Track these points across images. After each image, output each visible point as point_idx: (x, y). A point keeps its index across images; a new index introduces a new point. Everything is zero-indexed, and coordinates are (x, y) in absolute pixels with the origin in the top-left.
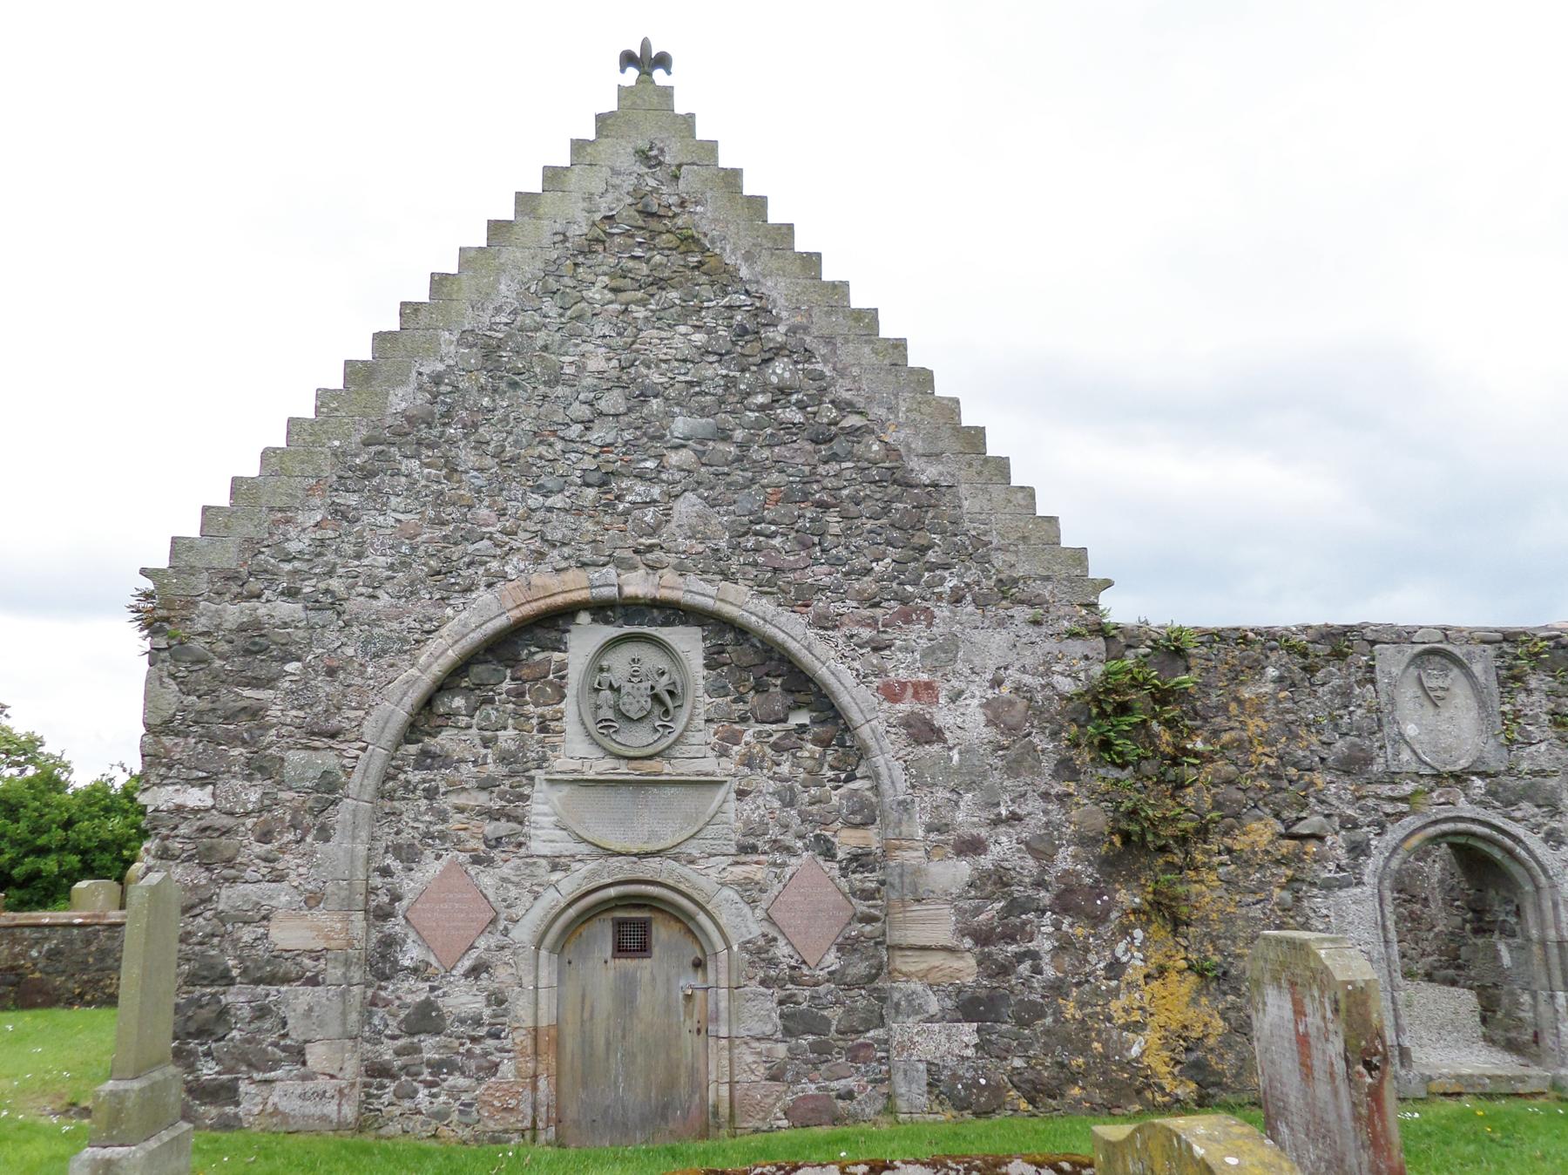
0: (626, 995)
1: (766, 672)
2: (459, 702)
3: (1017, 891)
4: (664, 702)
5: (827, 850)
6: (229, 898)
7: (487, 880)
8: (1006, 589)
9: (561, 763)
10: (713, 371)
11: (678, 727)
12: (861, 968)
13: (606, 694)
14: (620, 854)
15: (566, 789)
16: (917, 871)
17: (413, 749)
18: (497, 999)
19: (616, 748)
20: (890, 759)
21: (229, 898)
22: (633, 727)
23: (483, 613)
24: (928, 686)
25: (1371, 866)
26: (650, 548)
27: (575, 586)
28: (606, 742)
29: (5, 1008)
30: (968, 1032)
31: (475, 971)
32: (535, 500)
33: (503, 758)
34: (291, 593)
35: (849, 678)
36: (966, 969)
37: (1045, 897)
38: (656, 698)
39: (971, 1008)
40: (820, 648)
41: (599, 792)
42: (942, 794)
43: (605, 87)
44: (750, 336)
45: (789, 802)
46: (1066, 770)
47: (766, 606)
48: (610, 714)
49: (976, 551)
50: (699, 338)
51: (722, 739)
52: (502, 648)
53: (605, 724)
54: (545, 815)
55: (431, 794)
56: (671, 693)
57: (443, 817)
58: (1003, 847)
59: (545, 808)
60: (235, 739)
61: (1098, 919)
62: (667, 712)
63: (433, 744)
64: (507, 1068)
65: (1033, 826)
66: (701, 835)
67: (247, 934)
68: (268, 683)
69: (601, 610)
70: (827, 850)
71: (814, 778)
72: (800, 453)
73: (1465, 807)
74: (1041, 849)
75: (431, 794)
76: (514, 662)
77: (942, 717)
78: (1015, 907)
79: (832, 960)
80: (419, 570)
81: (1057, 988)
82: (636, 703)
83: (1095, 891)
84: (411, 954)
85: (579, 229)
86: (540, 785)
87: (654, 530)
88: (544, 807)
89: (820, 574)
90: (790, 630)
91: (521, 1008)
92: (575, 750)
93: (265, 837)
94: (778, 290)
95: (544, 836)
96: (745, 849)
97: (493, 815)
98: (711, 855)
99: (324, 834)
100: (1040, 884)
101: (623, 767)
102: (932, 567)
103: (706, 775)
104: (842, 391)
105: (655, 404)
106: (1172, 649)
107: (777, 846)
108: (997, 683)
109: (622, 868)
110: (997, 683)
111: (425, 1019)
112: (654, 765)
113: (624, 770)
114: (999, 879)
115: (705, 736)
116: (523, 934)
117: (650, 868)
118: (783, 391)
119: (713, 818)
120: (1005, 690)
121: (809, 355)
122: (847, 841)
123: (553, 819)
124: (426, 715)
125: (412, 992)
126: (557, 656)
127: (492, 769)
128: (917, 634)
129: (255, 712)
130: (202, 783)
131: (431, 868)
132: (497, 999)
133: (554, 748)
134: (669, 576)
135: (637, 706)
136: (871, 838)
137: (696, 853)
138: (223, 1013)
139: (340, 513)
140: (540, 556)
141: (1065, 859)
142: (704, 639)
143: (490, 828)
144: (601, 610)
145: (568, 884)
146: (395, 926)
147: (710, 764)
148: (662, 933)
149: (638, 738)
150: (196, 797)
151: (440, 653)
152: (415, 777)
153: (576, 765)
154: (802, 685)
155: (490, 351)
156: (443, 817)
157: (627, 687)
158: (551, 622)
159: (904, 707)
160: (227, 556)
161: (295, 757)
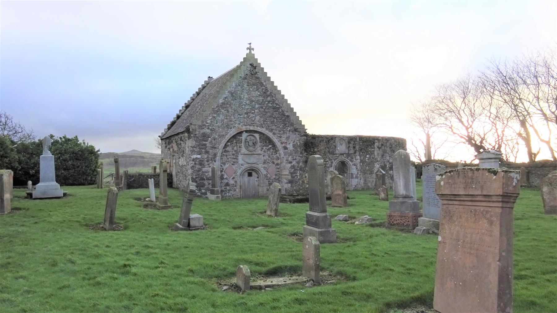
0: (249, 182)
1: (267, 141)
4: (254, 144)
5: (273, 163)
6: (204, 169)
7: (234, 167)
8: (296, 130)
9: (242, 152)
10: (261, 98)
12: (277, 177)
18: (236, 182)
20: (281, 151)
21: (204, 169)
23: (233, 132)
27: (244, 128)
29: (509, 188)
30: (290, 185)
31: (233, 178)
32: (239, 116)
33: (235, 151)
34: (208, 128)
36: (290, 177)
39: (290, 182)
43: (244, 53)
45: (269, 157)
46: (301, 153)
47: (267, 132)
49: (292, 125)
52: (234, 137)
55: (226, 156)
57: (228, 159)
58: (294, 163)
60: (203, 149)
61: (304, 171)
64: (237, 190)
65: (297, 160)
67: (206, 174)
68: (207, 141)
69: (246, 131)
70: (273, 163)
71: (272, 154)
73: (343, 158)
74: (298, 163)
75: (226, 156)
76: (236, 138)
77: (288, 146)
78: (296, 170)
79: (274, 177)
81: (299, 179)
82: (251, 143)
83: (304, 168)
84: (225, 176)
85: (243, 76)
87: (254, 121)
88: (240, 157)
89: (274, 127)
90: (270, 135)
91: (238, 182)
92: (244, 150)
93: (208, 161)
94: (269, 86)
95: (240, 161)
96: (264, 163)
97: (234, 159)
99: (215, 161)
104: (277, 102)
106: (314, 137)
107: (268, 163)
109: (250, 165)
111: (227, 184)
113: (250, 153)
114: (293, 167)
115: (259, 148)
116: (238, 174)
117: (253, 165)
118: (269, 102)
119: (259, 158)
121: (273, 96)
122: (276, 162)
125: (226, 181)
127: (234, 152)
128: (285, 136)
129: (205, 145)
131: (227, 166)
132: (236, 182)
134: (256, 127)
136: (279, 161)
138: (204, 184)
139: (214, 117)
140: (239, 124)
141: (301, 164)
143: (234, 160)
144: (246, 131)
145: (243, 168)
146: (223, 173)
147: (260, 152)
148: (254, 173)
149: (251, 148)
150: (199, 156)
151: (228, 137)
154: (271, 142)
155: (232, 94)
156: (228, 159)
158: (240, 133)
161: (211, 151)
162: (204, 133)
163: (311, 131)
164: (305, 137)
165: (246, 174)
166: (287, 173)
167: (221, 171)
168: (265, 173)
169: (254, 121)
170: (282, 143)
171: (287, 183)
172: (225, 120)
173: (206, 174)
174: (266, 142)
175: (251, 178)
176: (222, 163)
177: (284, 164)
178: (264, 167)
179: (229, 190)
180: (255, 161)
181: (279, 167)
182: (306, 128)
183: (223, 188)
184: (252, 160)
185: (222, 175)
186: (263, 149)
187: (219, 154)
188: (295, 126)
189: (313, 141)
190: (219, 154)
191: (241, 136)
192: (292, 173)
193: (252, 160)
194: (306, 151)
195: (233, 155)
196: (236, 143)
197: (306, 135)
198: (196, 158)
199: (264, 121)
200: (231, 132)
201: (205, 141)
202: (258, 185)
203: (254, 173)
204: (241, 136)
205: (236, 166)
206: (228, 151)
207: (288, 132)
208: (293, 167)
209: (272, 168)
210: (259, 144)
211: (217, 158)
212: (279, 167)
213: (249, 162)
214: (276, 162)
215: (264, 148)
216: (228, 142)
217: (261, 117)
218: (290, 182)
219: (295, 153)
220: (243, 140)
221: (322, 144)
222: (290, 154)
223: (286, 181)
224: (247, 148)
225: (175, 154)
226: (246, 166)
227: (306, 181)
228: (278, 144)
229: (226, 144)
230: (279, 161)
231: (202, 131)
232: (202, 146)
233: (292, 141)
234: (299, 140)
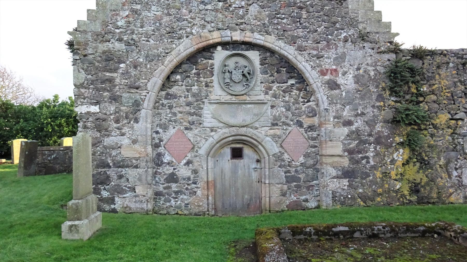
0: (234, 171)
3: (363, 138)
4: (247, 76)
5: (300, 124)
6: (108, 141)
7: (190, 135)
8: (363, 37)
9: (213, 97)
11: (252, 85)
12: (311, 162)
13: (227, 74)
14: (233, 126)
15: (215, 106)
17: (164, 93)
18: (195, 172)
19: (231, 92)
20: (322, 94)
21: (108, 141)
22: (236, 84)
23: (185, 48)
24: (336, 70)
26: (242, 23)
27: (216, 37)
28: (227, 90)
30: (345, 182)
31: (188, 163)
32: (202, 7)
33: (194, 95)
34: (120, 40)
35: (309, 68)
36: (345, 162)
37: (372, 139)
38: (244, 75)
39: (347, 174)
40: (299, 58)
41: (226, 105)
42: (339, 106)
45: (288, 109)
46: (380, 98)
47: (281, 43)
48: (228, 81)
49: (353, 23)
51: (266, 89)
52: (192, 58)
53: (227, 84)
54: (208, 114)
55: (171, 107)
56: (249, 73)
57: (175, 114)
58: (359, 124)
59: (208, 112)
60: (105, 90)
62: (248, 80)
63: (171, 91)
64: (199, 192)
66: (260, 120)
67: (114, 153)
69: (225, 45)
70: (300, 124)
71: (296, 102)
74: (371, 123)
75: (171, 107)
76: (196, 63)
77: (340, 80)
79: (302, 159)
81: (374, 168)
82: (237, 76)
83: (388, 137)
84: (167, 158)
86: (207, 104)
87: (242, 17)
88: (208, 111)
89: (300, 32)
90: (289, 52)
91: (202, 174)
92: (217, 92)
93: (117, 121)
95: (208, 119)
96: (273, 125)
97: (192, 114)
98: (262, 127)
99: (137, 121)
100: (370, 135)
101: (234, 98)
103: (261, 100)
106: (419, 54)
107: (284, 123)
108: (358, 69)
109: (234, 131)
110: (358, 69)
111: (172, 178)
114: (356, 134)
115: (260, 88)
116: (202, 152)
117: (243, 131)
119: (260, 112)
120: (361, 71)
122: (307, 122)
123: (211, 115)
124: (168, 81)
125: (168, 170)
126: (210, 61)
127: (190, 99)
128: (332, 53)
129: (111, 80)
130: (97, 103)
131: (172, 131)
132: (195, 172)
133: (210, 92)
134: (248, 34)
135: (238, 78)
136: (316, 121)
137: (258, 126)
138: (108, 177)
139: (135, 12)
140: (204, 27)
142: (260, 55)
143: (190, 118)
144: (225, 45)
145: (216, 136)
146: (161, 150)
147: (262, 97)
149: (238, 89)
152: (165, 102)
153: (218, 98)
154: (292, 70)
157: (234, 72)
158: (208, 50)
159: (327, 77)
162: (109, 51)
163: (407, 41)
164: (392, 56)
165: (228, 151)
166: (339, 150)
167: (156, 146)
168: (276, 149)
169: (242, 17)
170: (323, 73)
171: (337, 177)
172: (166, 19)
173: (114, 153)
174: (278, 72)
175: (240, 163)
176: (160, 126)
177: (330, 127)
178: (274, 137)
179: (176, 193)
180: (249, 119)
181: (315, 134)
182: (393, 31)
183: (161, 188)
184: (241, 117)
185: (159, 155)
186: (270, 89)
187: (147, 104)
188: (361, 27)
189: (417, 64)
190: (147, 104)
191: (211, 58)
192: (351, 152)
193: (241, 117)
194: (393, 92)
195: (189, 104)
196: (198, 74)
197: (396, 50)
198: (88, 113)
199: (271, 17)
200: (181, 47)
201: (111, 71)
202: (259, 181)
203: (247, 151)
204: (211, 58)
205: (196, 131)
206: (174, 96)
207: (341, 44)
208: (355, 135)
209: (296, 137)
210: (259, 76)
211: (143, 112)
212: (315, 134)
213: (232, 121)
214: (307, 122)
215: (275, 86)
216: (173, 72)
217: (262, 7)
218: (347, 174)
219: (362, 98)
220: (216, 68)
221: (443, 72)
222: (349, 102)
223: (334, 172)
224: (226, 86)
225: (457, 143)
226: (223, 132)
227: (393, 174)
228: (311, 75)
229: (168, 78)
230: (316, 121)
231: (102, 47)
232: (103, 82)
233: (355, 66)
234: (375, 65)
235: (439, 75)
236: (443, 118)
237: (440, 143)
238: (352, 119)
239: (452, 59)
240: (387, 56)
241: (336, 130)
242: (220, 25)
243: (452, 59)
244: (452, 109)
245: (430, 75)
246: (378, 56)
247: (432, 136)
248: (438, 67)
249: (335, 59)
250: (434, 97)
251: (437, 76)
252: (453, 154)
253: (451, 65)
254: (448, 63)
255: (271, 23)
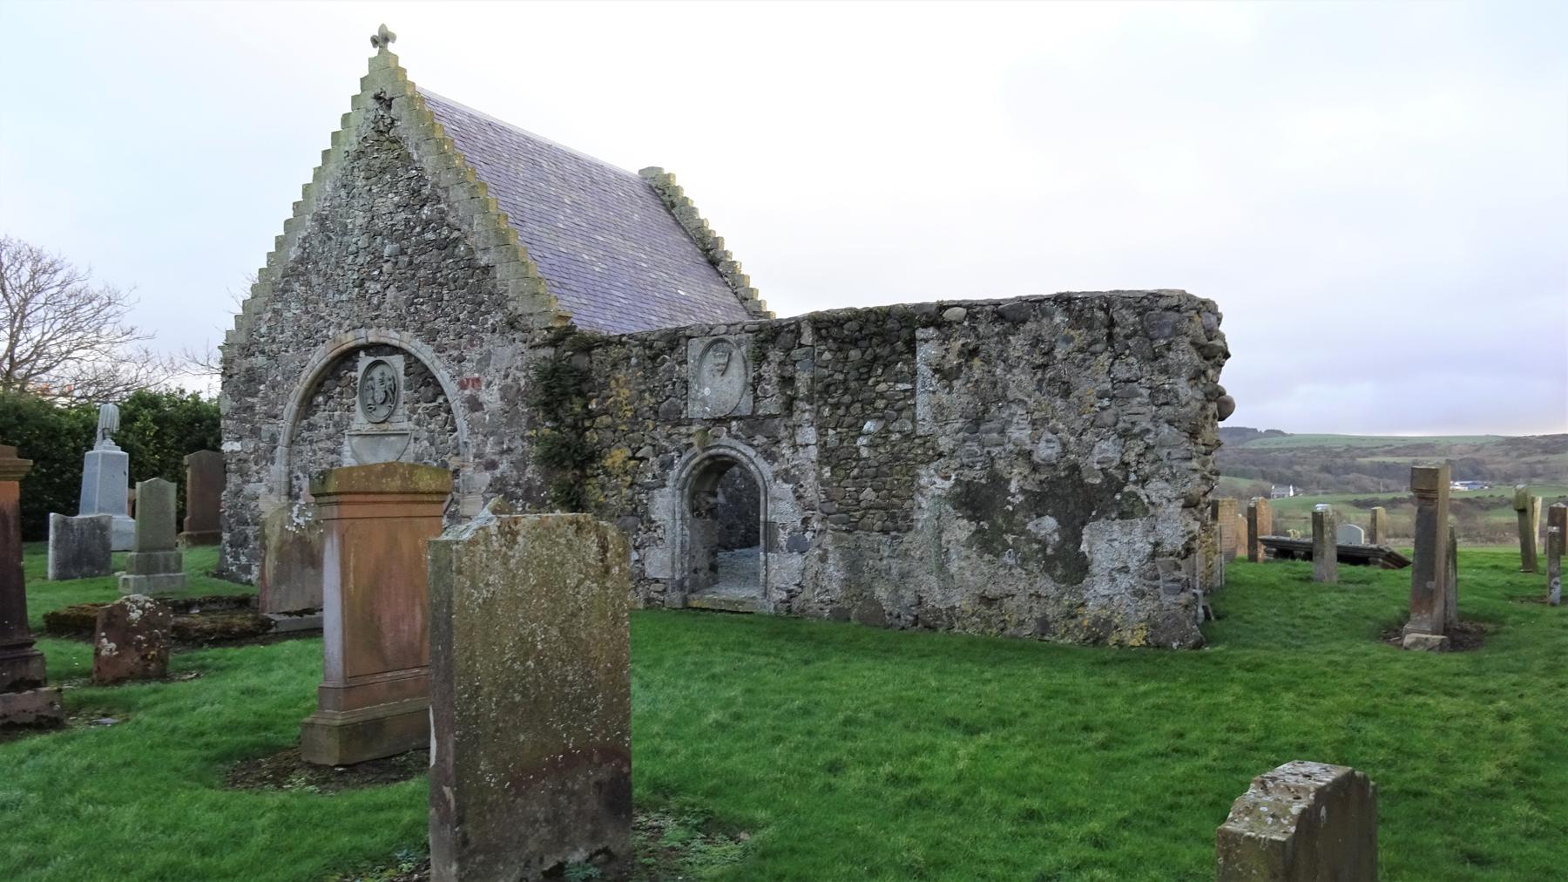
2: (321, 399)
3: (510, 489)
8: (512, 324)
9: (354, 426)
16: (470, 478)
17: (305, 422)
23: (318, 358)
24: (478, 380)
25: (672, 474)
26: (377, 317)
35: (447, 378)
37: (519, 492)
40: (437, 363)
42: (480, 437)
43: (358, 62)
44: (416, 197)
46: (532, 423)
47: (418, 342)
50: (396, 199)
63: (313, 419)
68: (254, 395)
72: (433, 256)
74: (520, 465)
77: (484, 396)
80: (301, 337)
83: (540, 489)
92: (360, 421)
100: (517, 485)
102: (483, 314)
105: (379, 239)
108: (506, 376)
110: (506, 376)
112: (384, 426)
120: (509, 380)
124: (307, 406)
128: (473, 354)
129: (251, 408)
130: (238, 440)
149: (383, 412)
151: (307, 376)
152: (305, 434)
156: (315, 452)
158: (347, 357)
159: (467, 392)
160: (242, 339)
169: (378, 307)
170: (463, 386)
172: (305, 318)
196: (341, 393)
210: (404, 394)
231: (246, 363)
235: (617, 380)
236: (617, 456)
237: (612, 501)
238: (496, 458)
239: (635, 350)
240: (542, 352)
241: (477, 476)
242: (356, 323)
243: (635, 350)
244: (634, 441)
245: (602, 380)
246: (529, 353)
247: (603, 487)
248: (615, 366)
249: (479, 361)
250: (606, 420)
251: (613, 383)
252: (631, 520)
253: (634, 361)
254: (629, 358)
255: (408, 312)
